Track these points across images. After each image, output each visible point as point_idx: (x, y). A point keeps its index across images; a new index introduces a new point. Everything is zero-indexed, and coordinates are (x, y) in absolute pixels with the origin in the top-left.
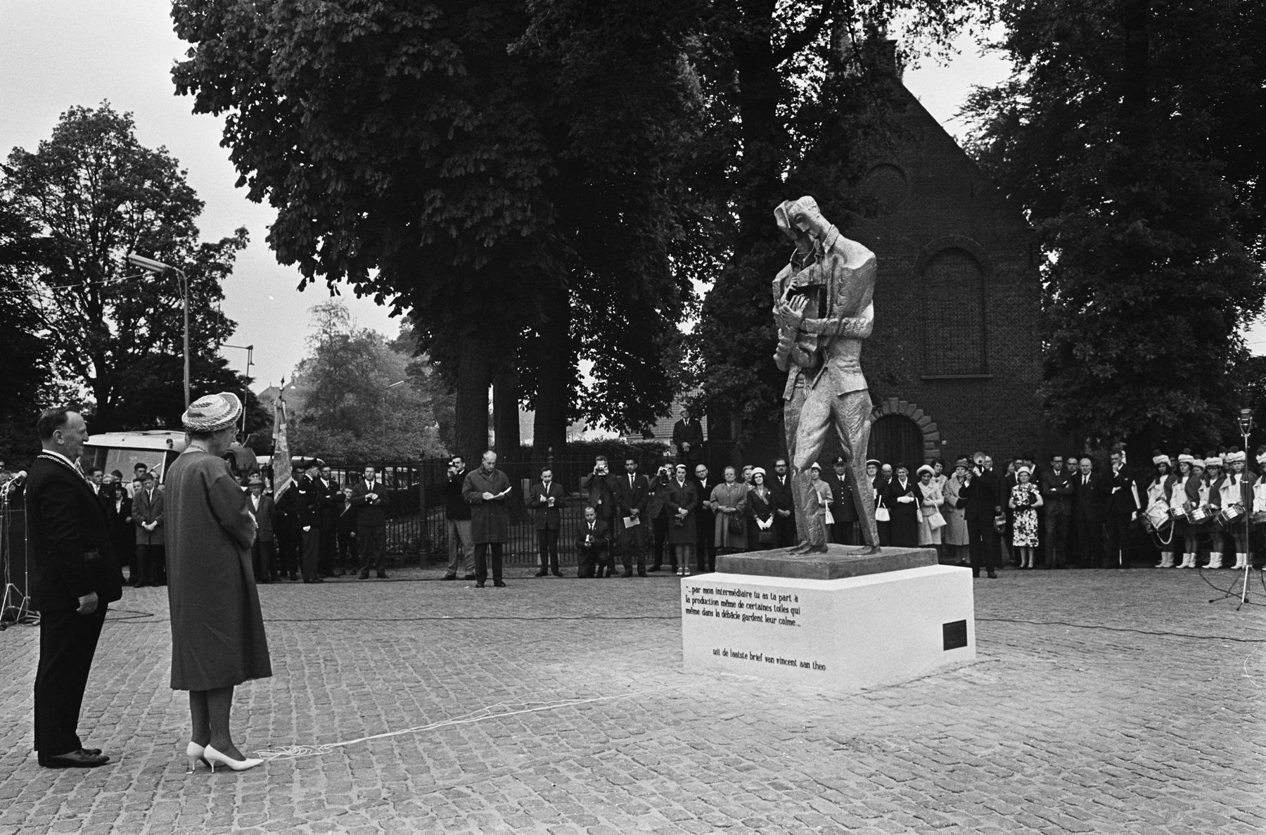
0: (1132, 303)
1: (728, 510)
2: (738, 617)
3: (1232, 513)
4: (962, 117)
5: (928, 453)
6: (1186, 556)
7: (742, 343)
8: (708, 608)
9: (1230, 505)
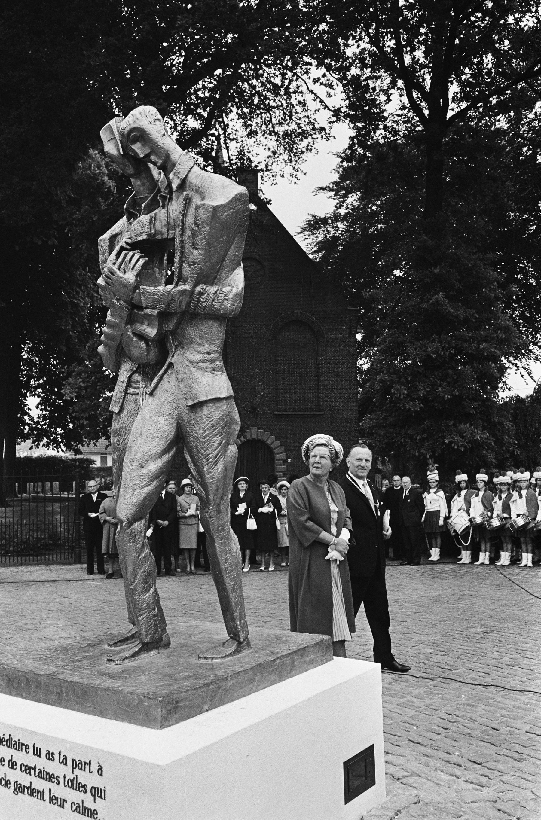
0: (434, 356)
3: (521, 522)
4: (302, 235)
6: (482, 555)
9: (518, 515)
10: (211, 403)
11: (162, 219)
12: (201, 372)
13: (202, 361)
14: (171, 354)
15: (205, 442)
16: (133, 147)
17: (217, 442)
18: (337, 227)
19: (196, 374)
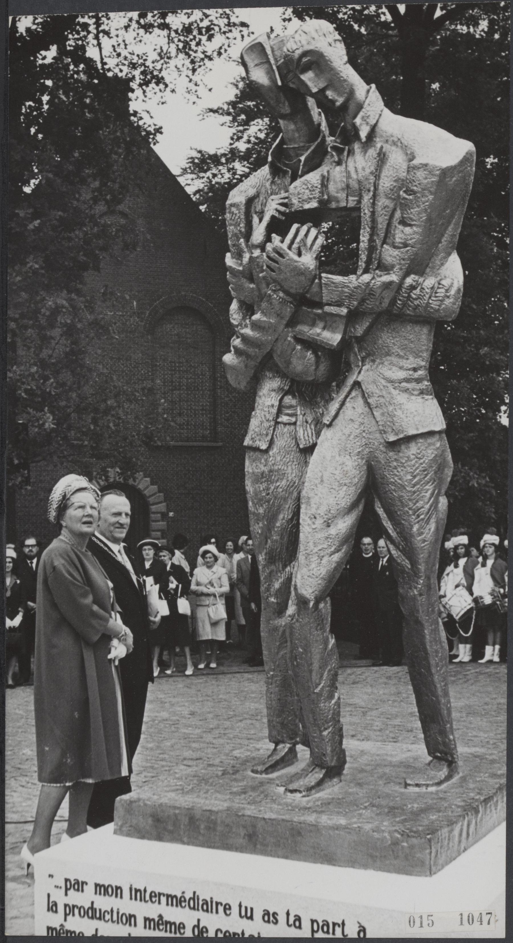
6: (489, 649)
10: (421, 438)
11: (338, 180)
12: (406, 395)
13: (407, 380)
15: (414, 492)
17: (430, 492)
18: (233, 169)
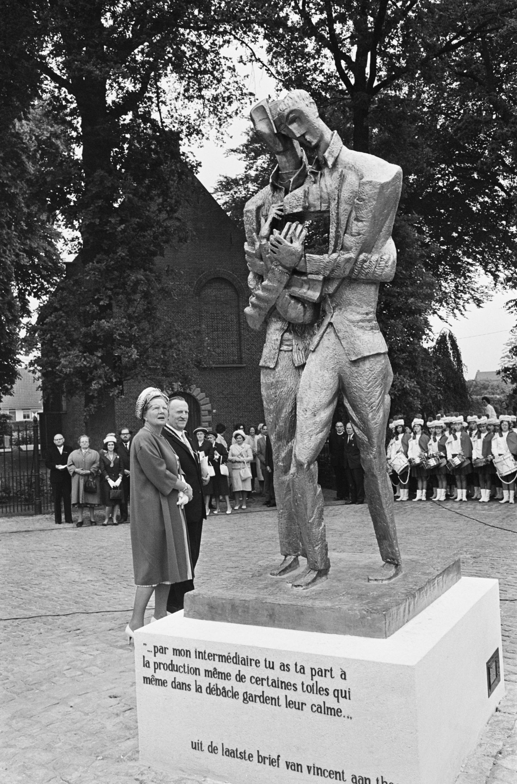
1: (82, 472)
2: (235, 695)
3: (457, 461)
5: (204, 418)
6: (419, 492)
7: (86, 335)
8: (182, 677)
9: (454, 456)
11: (315, 193)
13: (362, 321)
14: (330, 315)
15: (369, 393)
16: (290, 127)
17: (379, 392)
19: (357, 332)
